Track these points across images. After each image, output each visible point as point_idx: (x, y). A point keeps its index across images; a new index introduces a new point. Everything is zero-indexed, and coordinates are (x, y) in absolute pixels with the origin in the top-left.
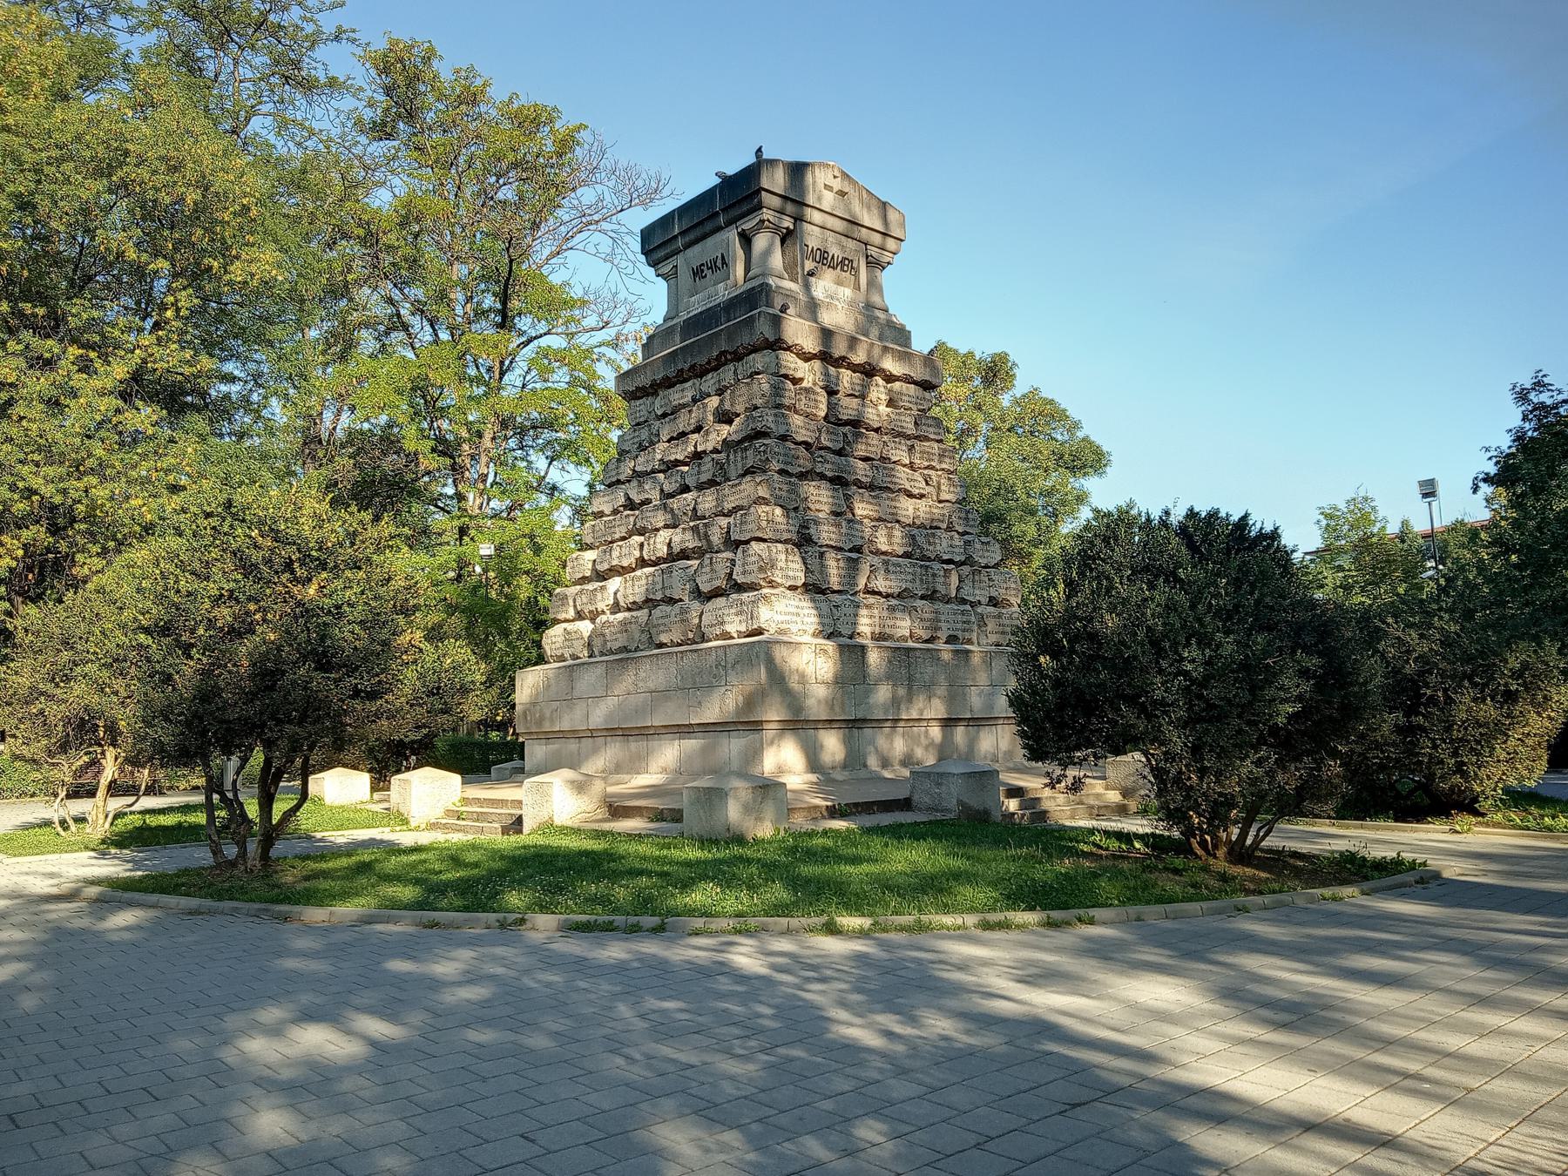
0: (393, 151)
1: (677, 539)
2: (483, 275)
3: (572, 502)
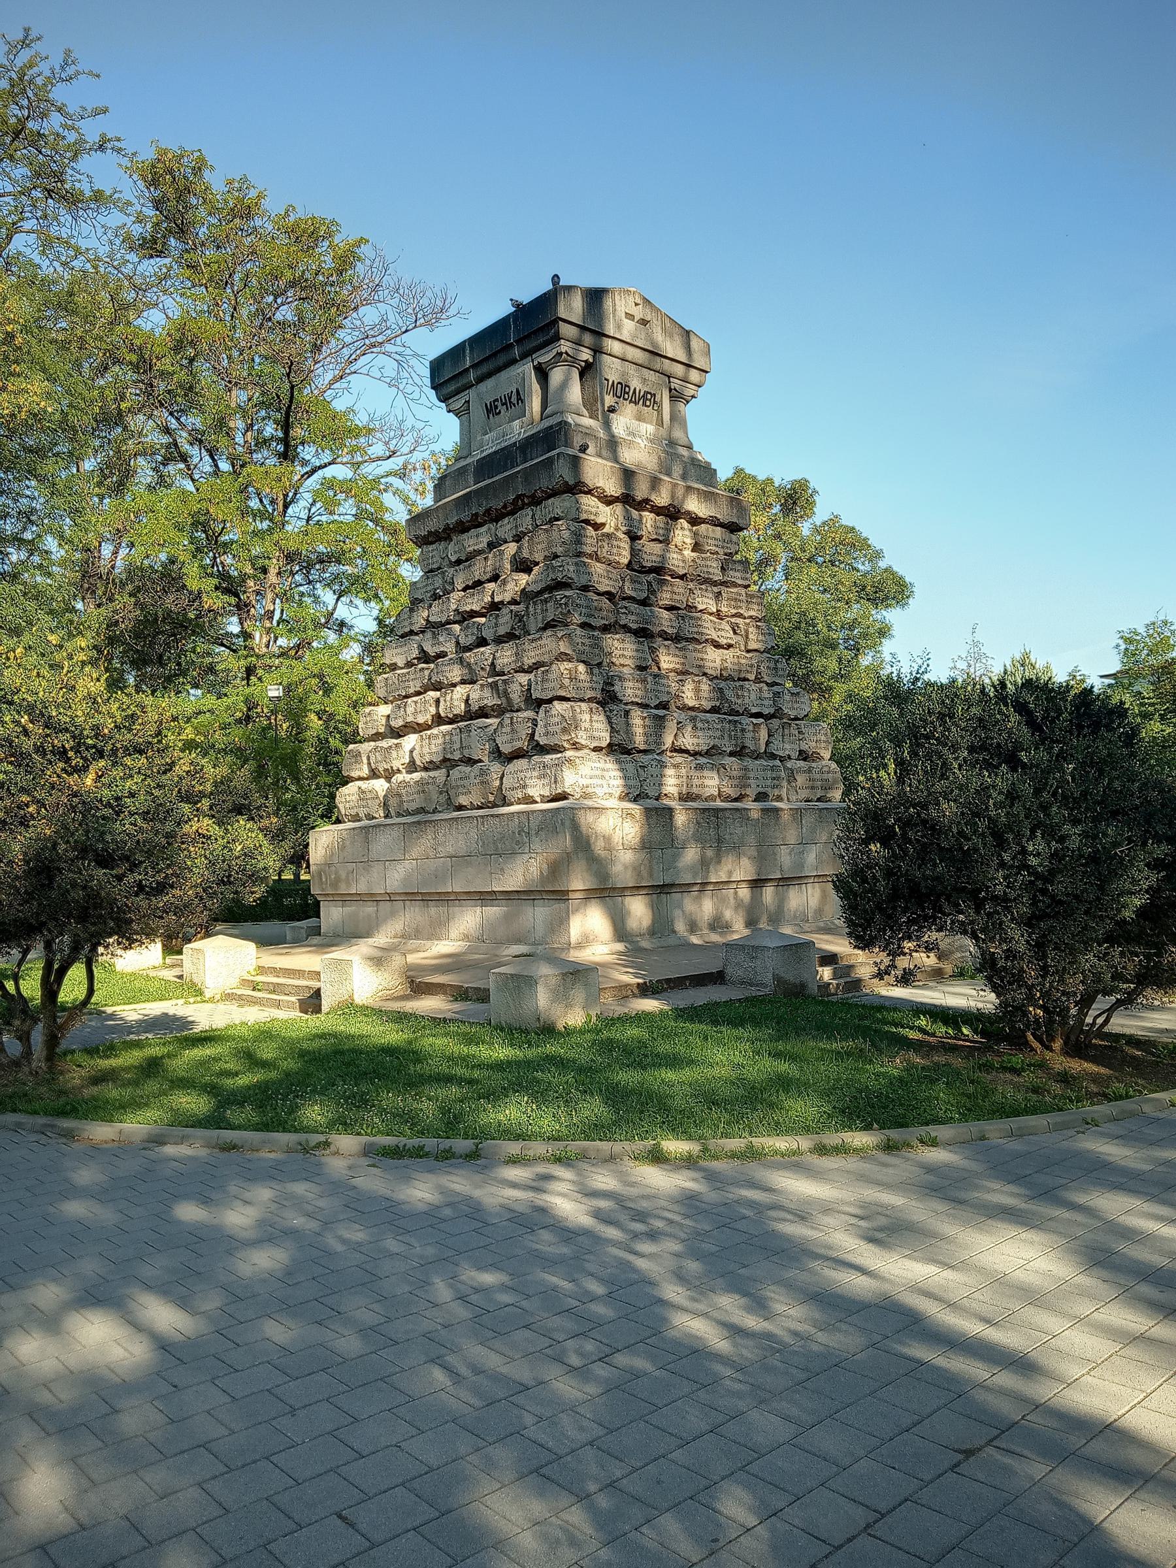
0: (164, 270)
1: (474, 696)
2: (263, 403)
3: (362, 638)
